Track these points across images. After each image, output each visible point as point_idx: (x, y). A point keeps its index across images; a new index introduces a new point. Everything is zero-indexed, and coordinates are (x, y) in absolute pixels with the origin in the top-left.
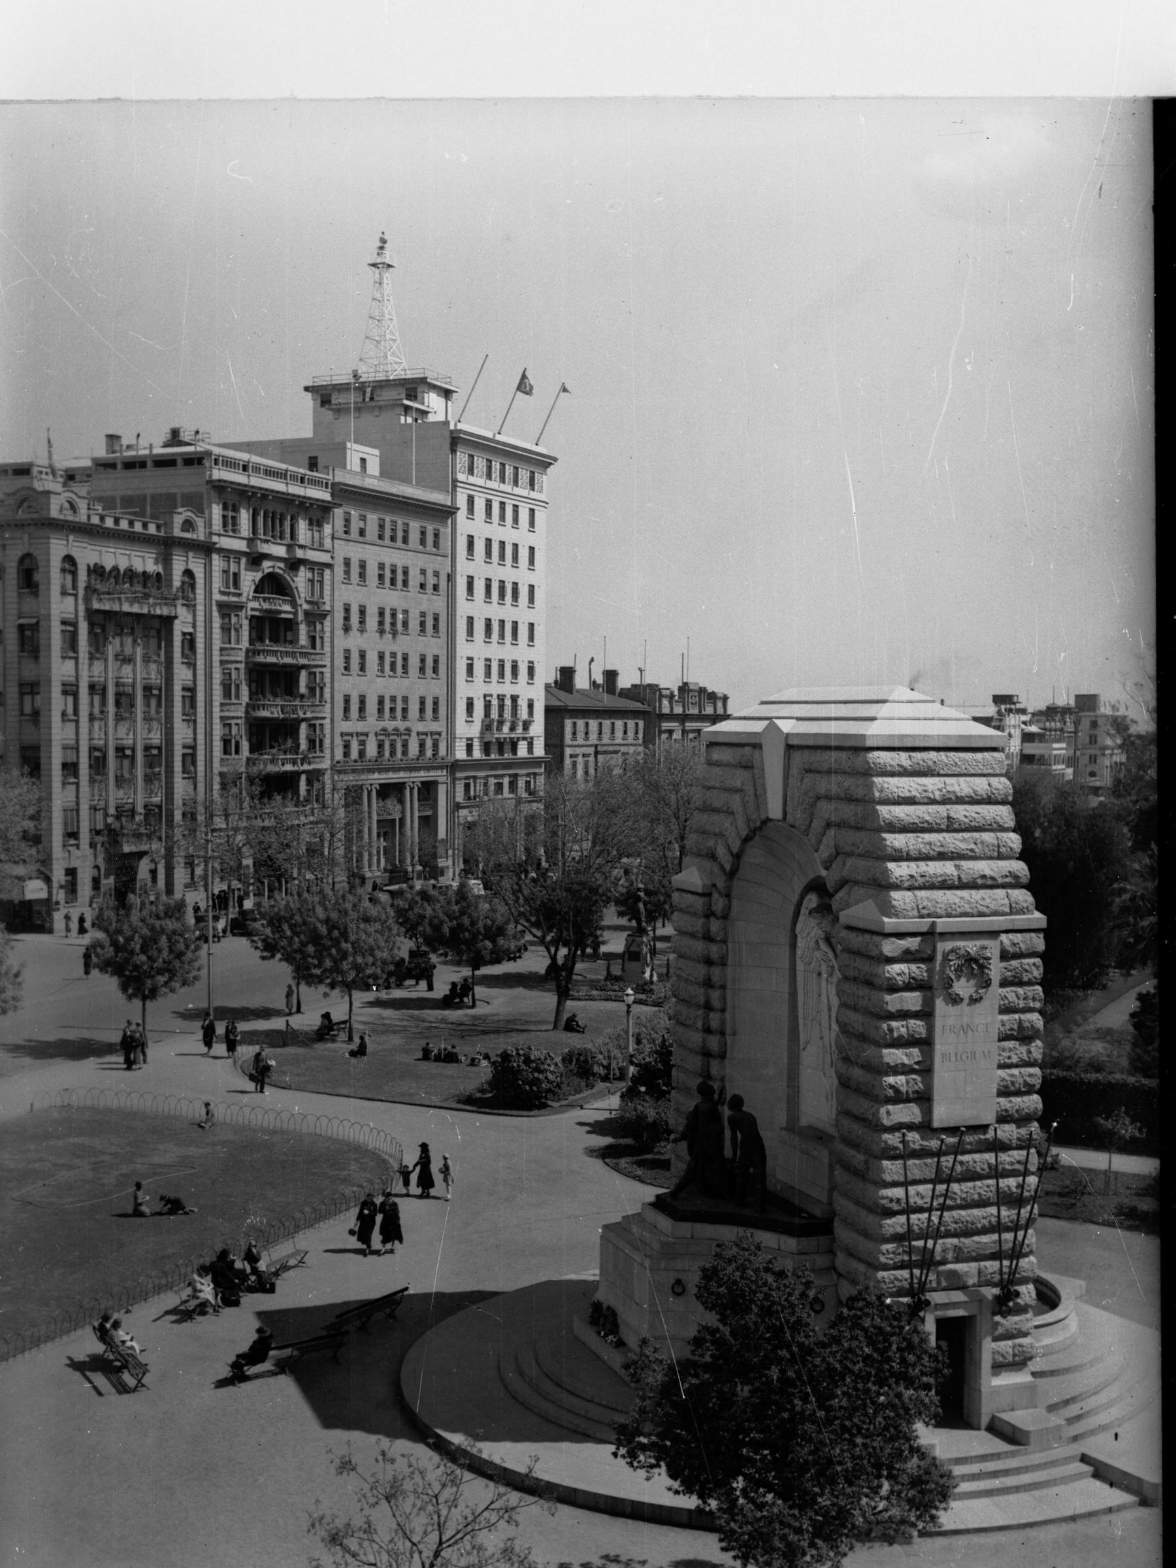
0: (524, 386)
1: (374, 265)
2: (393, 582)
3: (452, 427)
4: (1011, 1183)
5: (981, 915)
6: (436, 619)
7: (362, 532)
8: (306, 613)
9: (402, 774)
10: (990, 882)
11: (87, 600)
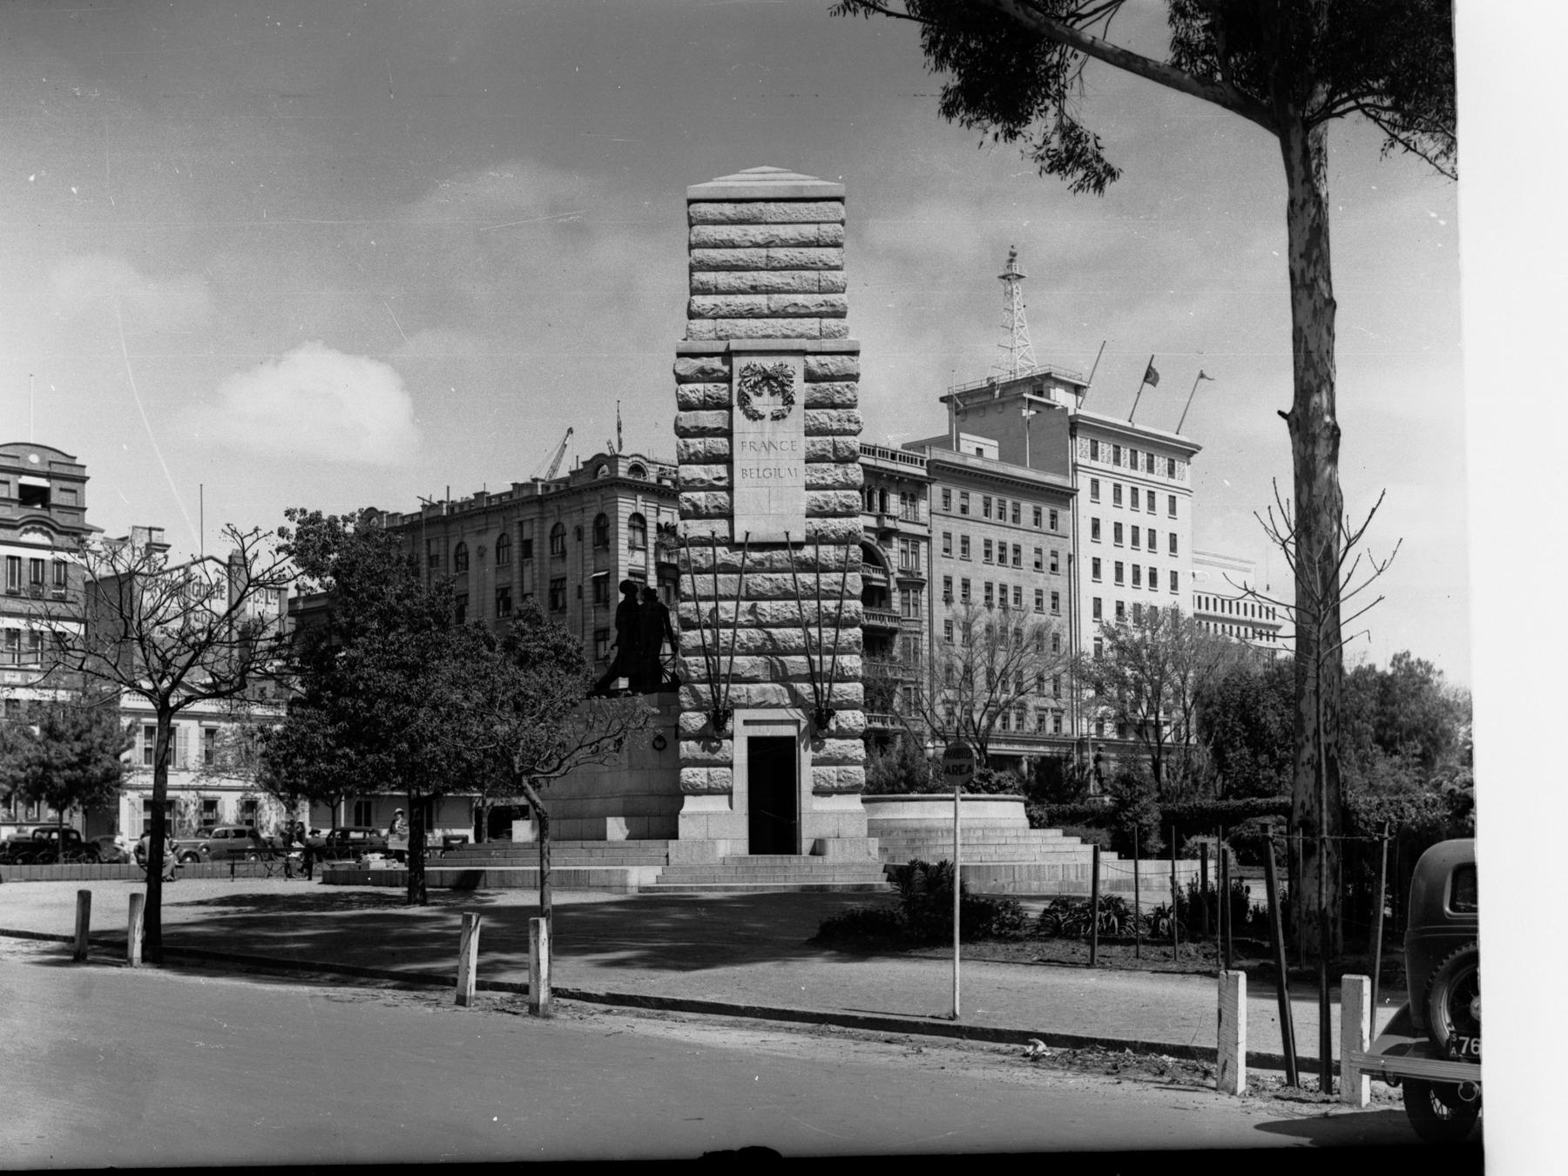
0: (1151, 376)
1: (1004, 277)
2: (1002, 559)
3: (1071, 413)
4: (830, 605)
5: (786, 337)
6: (1055, 597)
7: (964, 509)
8: (898, 581)
9: (1016, 747)
10: (803, 311)
11: (657, 554)
